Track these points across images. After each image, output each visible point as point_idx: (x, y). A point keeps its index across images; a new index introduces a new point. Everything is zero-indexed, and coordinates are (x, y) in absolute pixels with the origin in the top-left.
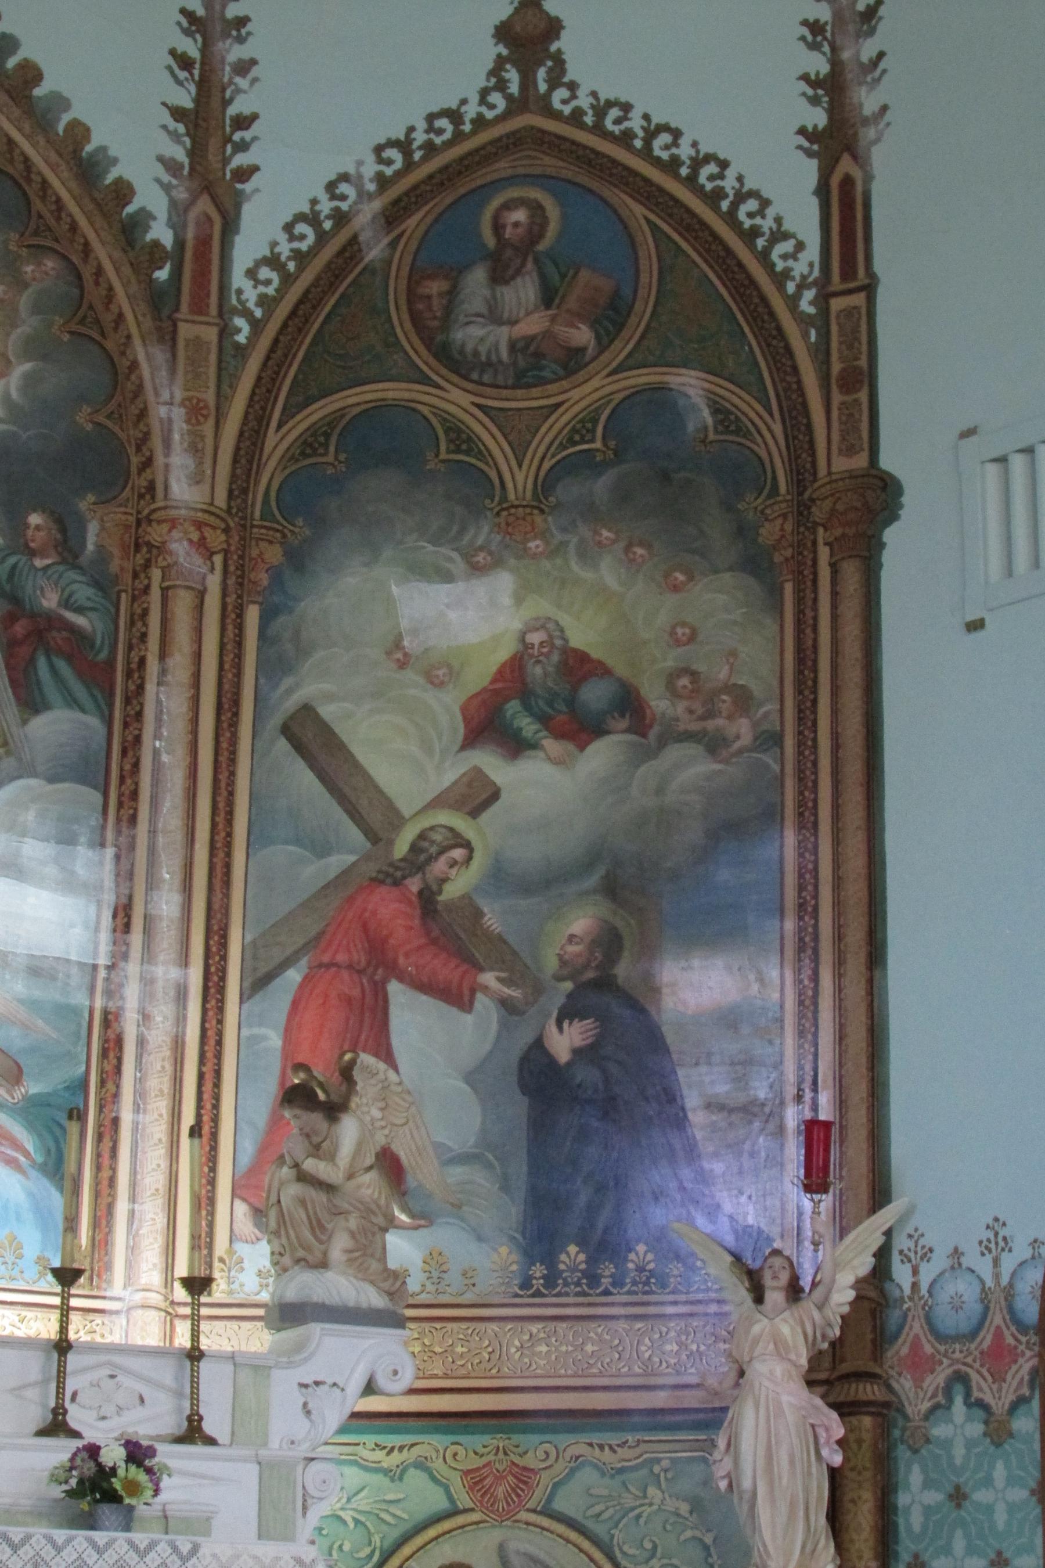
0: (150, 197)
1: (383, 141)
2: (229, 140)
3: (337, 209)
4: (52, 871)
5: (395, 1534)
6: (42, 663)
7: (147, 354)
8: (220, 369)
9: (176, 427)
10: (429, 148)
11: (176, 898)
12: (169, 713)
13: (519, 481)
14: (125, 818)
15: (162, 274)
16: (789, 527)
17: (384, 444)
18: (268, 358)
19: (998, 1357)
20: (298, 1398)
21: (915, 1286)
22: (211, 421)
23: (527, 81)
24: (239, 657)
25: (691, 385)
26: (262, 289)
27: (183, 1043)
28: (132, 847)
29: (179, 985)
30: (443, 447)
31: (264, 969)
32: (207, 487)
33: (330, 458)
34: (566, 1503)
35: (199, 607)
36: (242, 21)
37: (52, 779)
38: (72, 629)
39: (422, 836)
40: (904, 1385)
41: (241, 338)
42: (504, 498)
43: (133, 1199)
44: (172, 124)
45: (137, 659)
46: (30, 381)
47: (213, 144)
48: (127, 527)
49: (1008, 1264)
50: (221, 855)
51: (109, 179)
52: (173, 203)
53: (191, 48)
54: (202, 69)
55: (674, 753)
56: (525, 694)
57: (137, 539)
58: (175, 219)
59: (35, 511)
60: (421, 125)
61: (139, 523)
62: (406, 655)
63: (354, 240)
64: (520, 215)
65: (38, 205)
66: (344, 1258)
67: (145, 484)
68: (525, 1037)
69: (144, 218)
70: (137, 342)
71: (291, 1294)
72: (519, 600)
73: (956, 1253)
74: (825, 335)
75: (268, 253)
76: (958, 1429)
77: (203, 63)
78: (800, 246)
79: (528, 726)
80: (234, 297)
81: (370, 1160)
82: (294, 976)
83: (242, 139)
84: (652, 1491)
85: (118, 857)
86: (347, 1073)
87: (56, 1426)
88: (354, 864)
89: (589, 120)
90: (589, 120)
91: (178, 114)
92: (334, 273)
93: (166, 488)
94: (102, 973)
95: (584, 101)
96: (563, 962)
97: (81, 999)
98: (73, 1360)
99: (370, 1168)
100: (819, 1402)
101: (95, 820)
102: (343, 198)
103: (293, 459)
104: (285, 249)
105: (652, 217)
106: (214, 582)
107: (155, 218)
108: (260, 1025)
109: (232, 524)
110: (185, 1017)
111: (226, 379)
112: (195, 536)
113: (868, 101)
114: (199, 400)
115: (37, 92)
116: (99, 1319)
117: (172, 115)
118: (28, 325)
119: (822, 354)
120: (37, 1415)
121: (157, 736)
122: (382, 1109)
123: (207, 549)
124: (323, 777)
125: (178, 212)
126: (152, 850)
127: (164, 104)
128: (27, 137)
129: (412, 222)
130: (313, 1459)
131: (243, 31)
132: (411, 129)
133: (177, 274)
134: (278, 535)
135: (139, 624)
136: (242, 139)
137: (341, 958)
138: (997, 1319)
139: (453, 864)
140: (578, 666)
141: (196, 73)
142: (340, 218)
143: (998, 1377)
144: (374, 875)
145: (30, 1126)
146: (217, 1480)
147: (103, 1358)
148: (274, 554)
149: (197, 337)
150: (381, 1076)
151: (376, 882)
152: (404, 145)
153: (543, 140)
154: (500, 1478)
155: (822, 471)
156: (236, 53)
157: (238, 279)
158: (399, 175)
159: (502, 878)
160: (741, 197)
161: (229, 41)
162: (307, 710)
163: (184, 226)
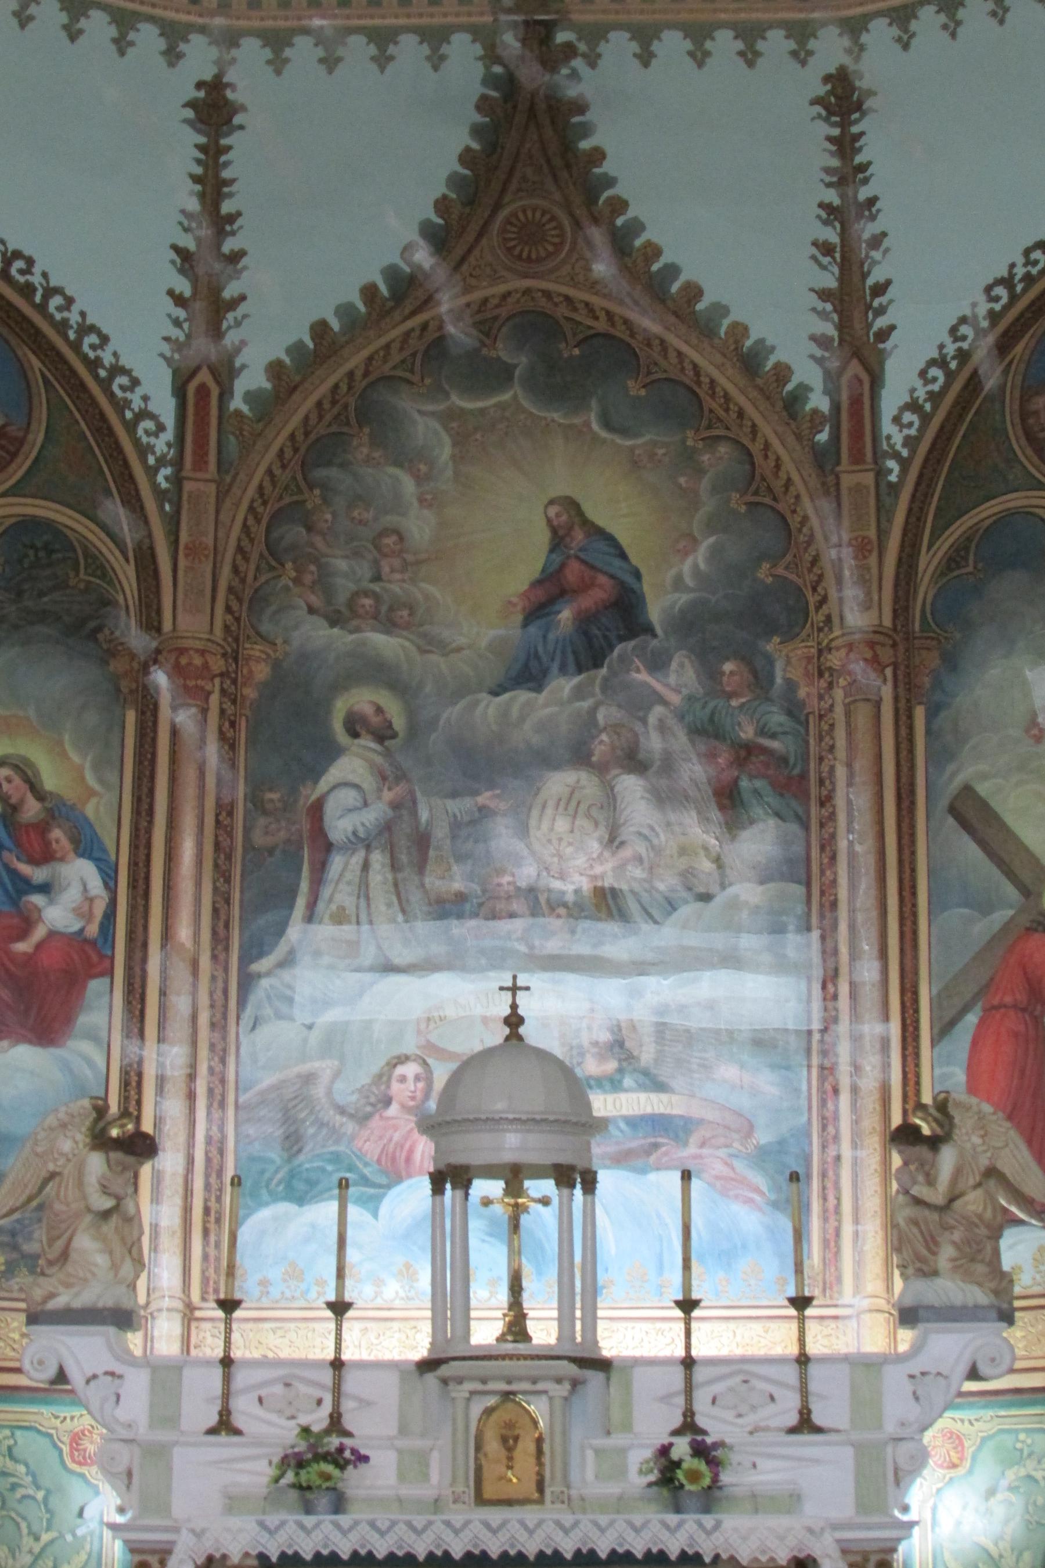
0: (807, 374)
1: (991, 281)
2: (869, 307)
3: (960, 350)
4: (766, 958)
7: (816, 510)
8: (878, 510)
9: (846, 566)
11: (876, 965)
12: (859, 811)
14: (827, 904)
15: (823, 437)
18: (916, 490)
20: (908, 1387)
22: (875, 554)
24: (911, 751)
26: (906, 431)
27: (890, 1086)
29: (883, 1038)
31: (948, 1015)
32: (875, 612)
33: (970, 569)
35: (877, 717)
41: (893, 478)
43: (856, 1221)
44: (820, 305)
45: (827, 769)
46: (715, 552)
47: (857, 315)
48: (809, 659)
50: (908, 923)
51: (769, 365)
52: (827, 375)
53: (831, 235)
54: (842, 251)
57: (819, 667)
58: (830, 386)
59: (727, 659)
60: (1020, 260)
61: (820, 652)
62: (1041, 730)
63: (975, 373)
65: (709, 403)
66: (950, 1265)
67: (823, 618)
69: (804, 389)
75: (909, 400)
77: (843, 246)
80: (885, 443)
82: (972, 1019)
83: (881, 305)
85: (823, 938)
88: (1012, 918)
91: (824, 295)
92: (962, 405)
93: (842, 618)
94: (816, 1037)
101: (800, 909)
102: (964, 338)
103: (943, 574)
106: (887, 692)
107: (811, 390)
108: (948, 1064)
109: (898, 639)
110: (889, 1065)
111: (884, 514)
112: (869, 655)
114: (864, 538)
115: (700, 306)
117: (820, 298)
118: (708, 505)
121: (850, 830)
122: (982, 1137)
123: (879, 663)
124: (983, 844)
125: (831, 380)
127: (812, 290)
128: (695, 348)
129: (1019, 349)
130: (901, 1439)
131: (874, 210)
132: (1013, 266)
133: (836, 437)
134: (935, 643)
135: (827, 739)
136: (881, 305)
137: (1008, 999)
141: (838, 255)
142: (963, 356)
144: (1028, 925)
146: (817, 1461)
147: (735, 1367)
148: (933, 660)
149: (858, 484)
150: (975, 1109)
152: (1007, 282)
156: (869, 230)
157: (888, 427)
158: (1006, 308)
161: (862, 222)
162: (968, 790)
163: (838, 389)
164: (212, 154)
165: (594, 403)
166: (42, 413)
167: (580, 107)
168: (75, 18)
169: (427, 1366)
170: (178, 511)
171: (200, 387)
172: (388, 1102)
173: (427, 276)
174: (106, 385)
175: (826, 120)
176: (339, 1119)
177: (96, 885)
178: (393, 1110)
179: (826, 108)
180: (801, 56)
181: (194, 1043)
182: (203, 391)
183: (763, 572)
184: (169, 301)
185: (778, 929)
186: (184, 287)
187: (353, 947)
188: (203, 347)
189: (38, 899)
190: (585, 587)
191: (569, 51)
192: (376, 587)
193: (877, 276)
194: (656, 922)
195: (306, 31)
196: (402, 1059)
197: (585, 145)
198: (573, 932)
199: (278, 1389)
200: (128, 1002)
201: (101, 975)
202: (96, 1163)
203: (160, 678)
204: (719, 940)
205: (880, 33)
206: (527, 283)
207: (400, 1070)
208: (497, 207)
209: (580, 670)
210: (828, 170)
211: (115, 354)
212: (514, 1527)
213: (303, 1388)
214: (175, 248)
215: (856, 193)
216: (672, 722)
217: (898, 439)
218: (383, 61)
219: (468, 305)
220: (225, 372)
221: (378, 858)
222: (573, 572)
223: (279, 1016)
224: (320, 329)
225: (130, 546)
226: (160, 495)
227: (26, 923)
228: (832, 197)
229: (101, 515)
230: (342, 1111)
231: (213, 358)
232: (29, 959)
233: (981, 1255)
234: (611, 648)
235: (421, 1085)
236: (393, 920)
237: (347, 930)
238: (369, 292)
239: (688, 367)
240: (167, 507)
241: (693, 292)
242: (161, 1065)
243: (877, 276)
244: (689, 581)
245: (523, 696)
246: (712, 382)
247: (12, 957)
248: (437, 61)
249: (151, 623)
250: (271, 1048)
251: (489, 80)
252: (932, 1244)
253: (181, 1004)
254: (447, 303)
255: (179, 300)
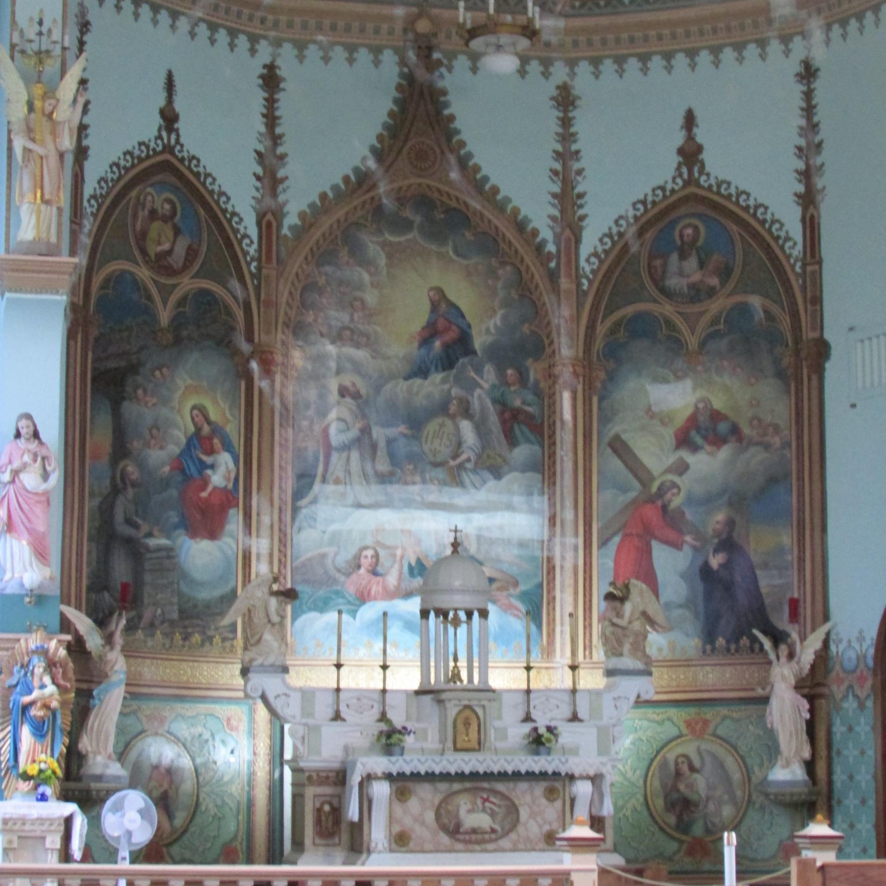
0: (546, 234)
5: (660, 744)
6: (516, 427)
10: (654, 203)
13: (693, 342)
15: (553, 265)
16: (792, 360)
17: (641, 328)
19: (862, 679)
21: (837, 653)
23: (690, 172)
24: (591, 417)
25: (756, 302)
28: (554, 493)
30: (664, 328)
34: (720, 732)
36: (577, 152)
37: (523, 471)
38: (526, 412)
39: (662, 484)
40: (834, 688)
41: (585, 288)
42: (687, 349)
44: (552, 200)
46: (504, 318)
49: (865, 646)
53: (558, 166)
55: (753, 450)
56: (698, 429)
60: (650, 193)
63: (626, 244)
64: (689, 231)
68: (699, 562)
69: (544, 241)
70: (544, 293)
71: (611, 666)
72: (694, 389)
73: (849, 641)
74: (804, 282)
76: (850, 704)
78: (795, 244)
79: (699, 440)
81: (637, 615)
82: (617, 539)
84: (750, 727)
85: (549, 499)
86: (627, 587)
87: (528, 718)
89: (715, 189)
90: (715, 189)
91: (554, 196)
95: (713, 181)
96: (714, 530)
97: (538, 553)
98: (532, 695)
99: (638, 618)
100: (799, 697)
101: (539, 485)
104: (600, 249)
105: (741, 232)
106: (580, 388)
113: (819, 183)
116: (551, 671)
118: (501, 294)
119: (804, 288)
120: (521, 714)
126: (562, 494)
133: (558, 264)
137: (634, 532)
138: (862, 666)
139: (674, 495)
140: (716, 416)
141: (561, 177)
142: (621, 235)
143: (862, 687)
145: (523, 602)
148: (602, 375)
151: (646, 502)
152: (644, 202)
153: (702, 200)
154: (697, 723)
155: (804, 337)
156: (576, 166)
157: (583, 263)
158: (642, 215)
159: (690, 500)
160: (773, 222)
162: (617, 437)
164: (271, 103)
165: (450, 243)
166: (205, 236)
167: (444, 93)
168: (212, 34)
169: (418, 693)
170: (260, 283)
171: (269, 220)
172: (359, 567)
173: (373, 173)
174: (229, 221)
175: (557, 108)
176: (338, 575)
177: (231, 464)
178: (362, 571)
179: (557, 102)
180: (546, 75)
181: (272, 539)
182: (269, 225)
183: (526, 329)
184: (254, 179)
185: (530, 494)
186: (259, 171)
187: (343, 495)
188: (268, 201)
189: (209, 472)
190: (447, 330)
191: (439, 63)
192: (352, 326)
193: (579, 189)
194: (476, 488)
195: (315, 42)
196: (366, 548)
197: (446, 112)
198: (441, 492)
199: (355, 701)
200: (245, 519)
201: (234, 506)
202: (273, 602)
203: (254, 365)
204: (504, 498)
205: (584, 69)
206: (419, 180)
207: (365, 553)
208: (406, 141)
209: (444, 370)
210: (557, 134)
211: (233, 206)
212: (474, 761)
213: (365, 701)
214: (256, 151)
215: (570, 148)
216: (484, 396)
217: (588, 269)
218: (351, 61)
219: (393, 189)
220: (279, 214)
221: (355, 455)
222: (441, 324)
223: (310, 526)
224: (323, 196)
225: (241, 301)
226: (252, 275)
227: (205, 482)
228: (559, 148)
229: (229, 286)
230: (339, 570)
231: (273, 207)
232: (207, 500)
233: (639, 648)
234: (457, 359)
235: (374, 560)
236: (361, 484)
237: (341, 488)
238: (346, 179)
239: (493, 227)
240: (255, 282)
241: (495, 190)
242: (258, 548)
243: (579, 189)
244: (493, 330)
245: (418, 381)
246: (504, 234)
247: (200, 499)
248: (377, 63)
249: (250, 339)
250: (308, 540)
251: (402, 75)
252: (620, 643)
253: (266, 520)
254: (383, 188)
255: (258, 178)
